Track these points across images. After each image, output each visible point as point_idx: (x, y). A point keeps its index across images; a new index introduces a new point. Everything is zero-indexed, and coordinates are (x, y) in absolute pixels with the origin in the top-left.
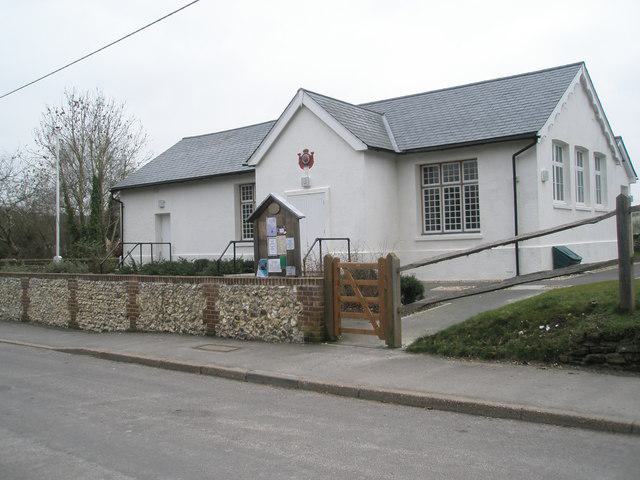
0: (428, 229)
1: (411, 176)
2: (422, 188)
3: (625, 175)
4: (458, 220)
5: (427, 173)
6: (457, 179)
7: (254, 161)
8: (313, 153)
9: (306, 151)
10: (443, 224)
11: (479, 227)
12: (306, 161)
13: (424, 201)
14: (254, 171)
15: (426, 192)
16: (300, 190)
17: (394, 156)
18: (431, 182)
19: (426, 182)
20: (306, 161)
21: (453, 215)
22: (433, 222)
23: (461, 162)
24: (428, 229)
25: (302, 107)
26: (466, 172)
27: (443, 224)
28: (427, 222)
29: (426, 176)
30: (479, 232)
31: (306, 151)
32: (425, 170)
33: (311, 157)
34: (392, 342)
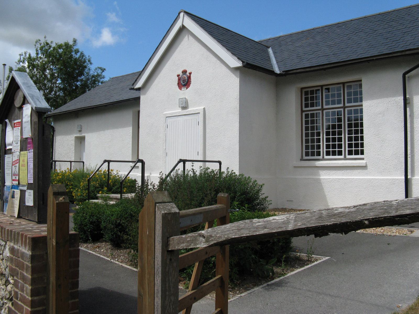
0: (307, 154)
1: (292, 99)
2: (302, 111)
3: (404, 194)
4: (340, 146)
5: (309, 97)
6: (339, 102)
7: (139, 84)
8: (190, 74)
9: (184, 72)
10: (323, 149)
11: (362, 153)
12: (184, 81)
13: (304, 144)
14: (137, 100)
15: (307, 116)
16: (179, 111)
17: (273, 77)
18: (312, 105)
19: (307, 106)
20: (184, 81)
21: (334, 140)
22: (313, 147)
23: (343, 84)
24: (307, 154)
25: (183, 28)
26: (349, 94)
27: (323, 149)
28: (307, 147)
29: (306, 99)
30: (363, 159)
31: (184, 72)
32: (306, 93)
33: (189, 78)
34: (82, 53)
